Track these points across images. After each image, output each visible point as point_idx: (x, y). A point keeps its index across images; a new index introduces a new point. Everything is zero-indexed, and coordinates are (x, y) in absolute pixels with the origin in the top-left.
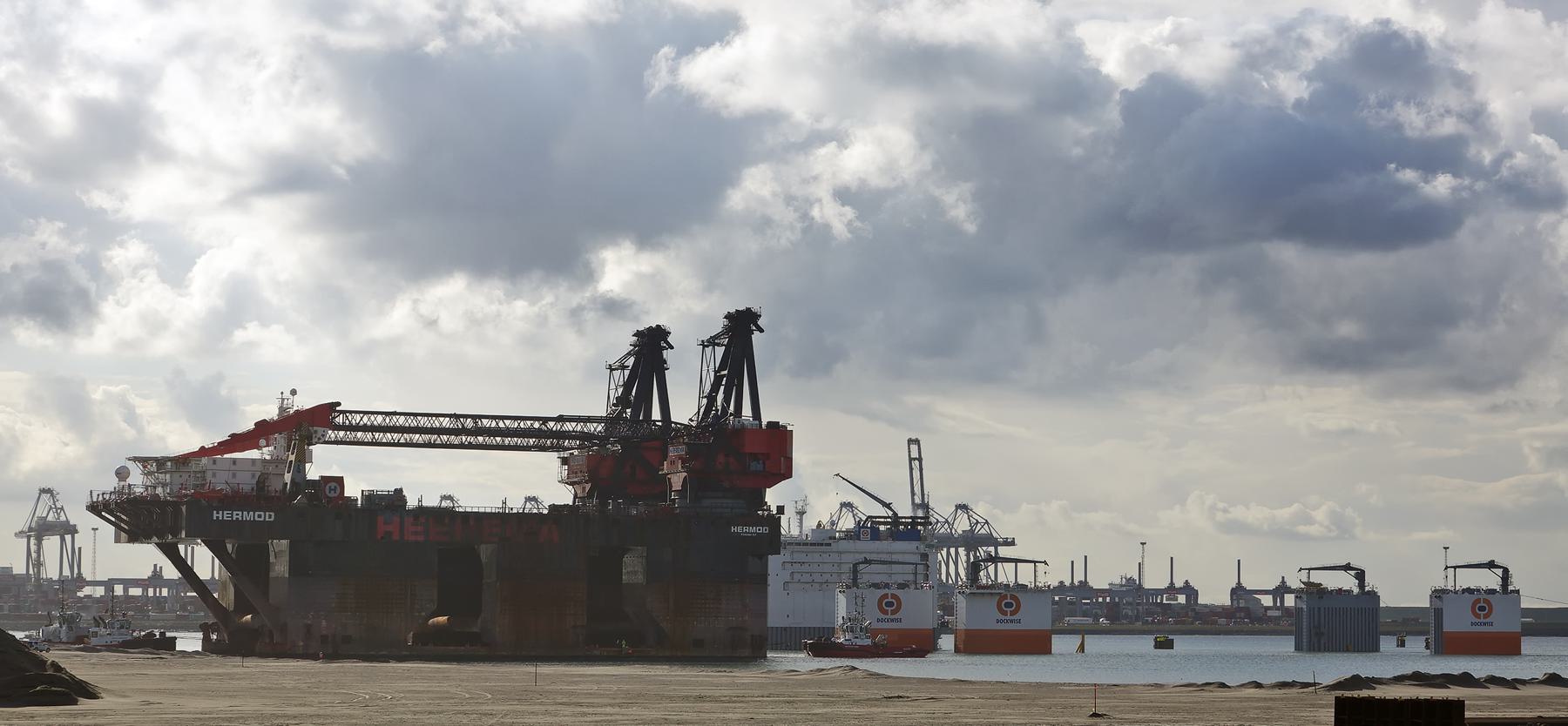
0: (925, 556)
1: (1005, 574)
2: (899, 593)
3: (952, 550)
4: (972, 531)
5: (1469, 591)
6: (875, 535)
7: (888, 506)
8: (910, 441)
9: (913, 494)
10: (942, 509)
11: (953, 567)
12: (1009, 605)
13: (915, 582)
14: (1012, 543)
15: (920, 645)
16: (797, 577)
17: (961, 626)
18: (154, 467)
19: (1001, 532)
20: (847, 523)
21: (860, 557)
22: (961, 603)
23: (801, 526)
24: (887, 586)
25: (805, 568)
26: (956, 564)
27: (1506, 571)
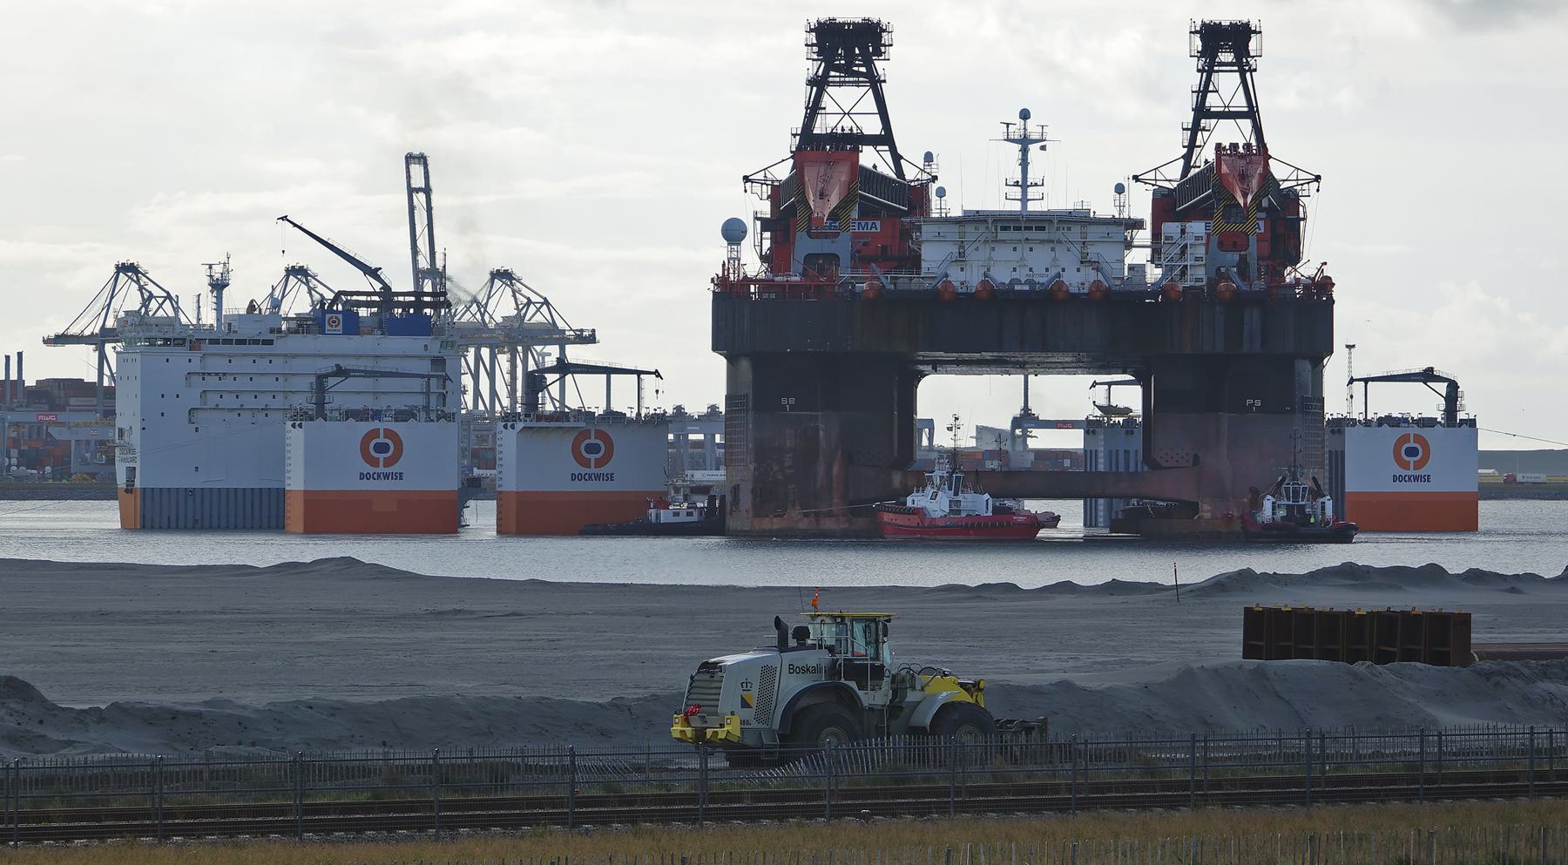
0: (439, 362)
1: (586, 394)
2: (399, 428)
3: (485, 352)
4: (520, 317)
5: (1388, 421)
6: (352, 324)
7: (373, 273)
8: (410, 159)
9: (415, 251)
10: (465, 268)
11: (487, 384)
12: (592, 449)
13: (427, 408)
14: (591, 339)
15: (438, 517)
16: (213, 399)
17: (510, 484)
19: (571, 318)
20: (298, 303)
21: (328, 365)
22: (508, 441)
23: (219, 308)
24: (377, 415)
25: (228, 383)
26: (491, 376)
27: (1453, 386)
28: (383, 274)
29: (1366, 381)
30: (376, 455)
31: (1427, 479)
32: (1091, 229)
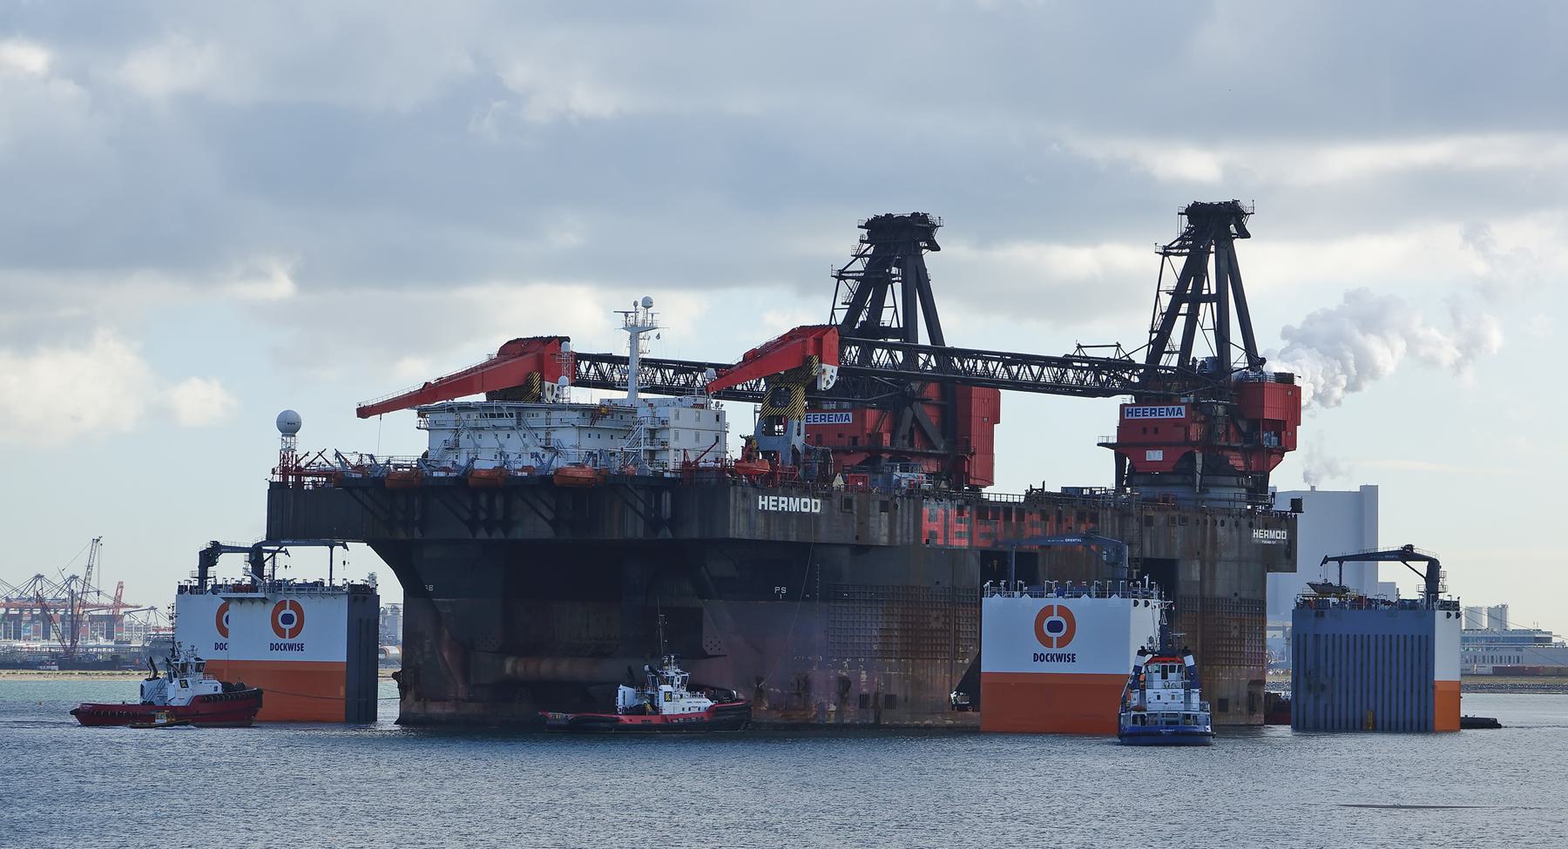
18: (588, 415)
27: (1434, 565)
28: (1419, 549)
29: (1341, 560)
30: (1049, 634)
31: (301, 647)
32: (555, 415)
